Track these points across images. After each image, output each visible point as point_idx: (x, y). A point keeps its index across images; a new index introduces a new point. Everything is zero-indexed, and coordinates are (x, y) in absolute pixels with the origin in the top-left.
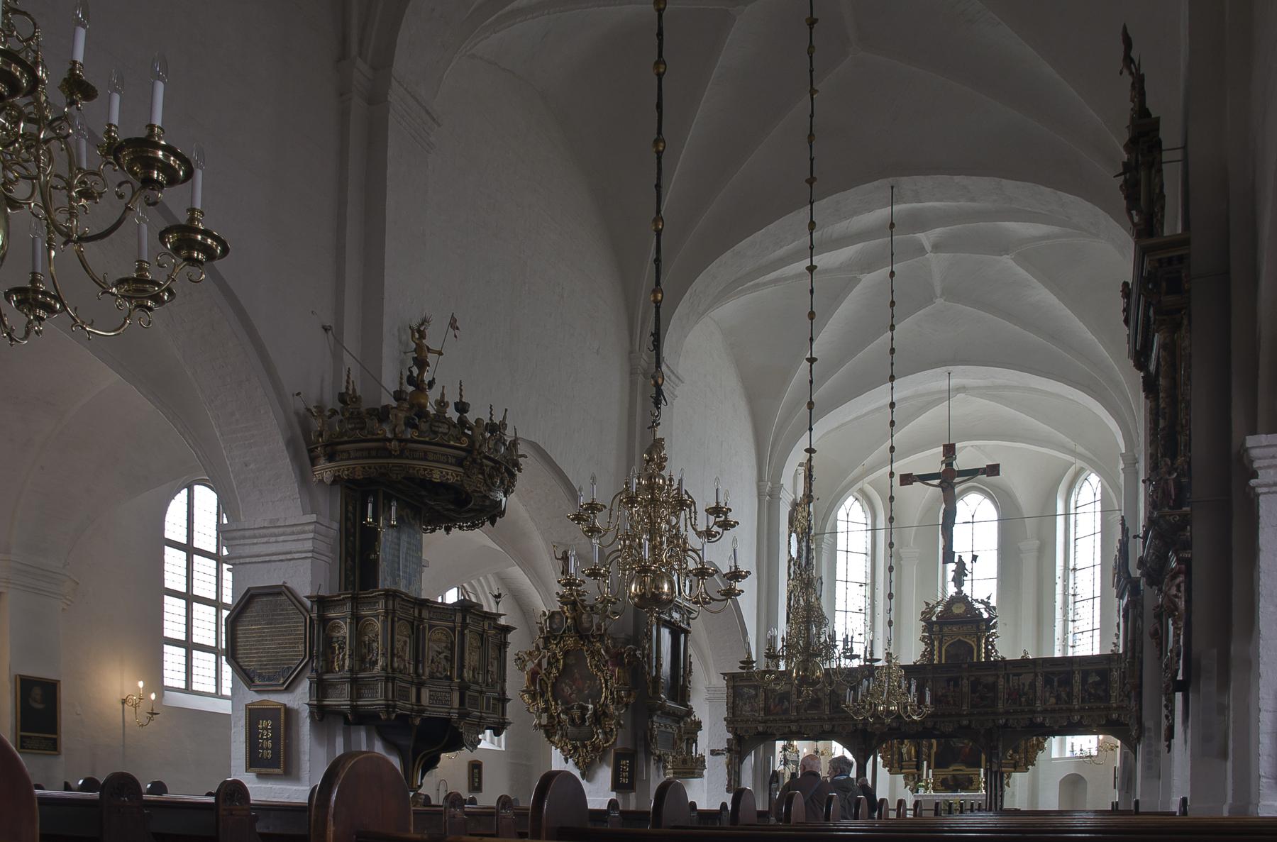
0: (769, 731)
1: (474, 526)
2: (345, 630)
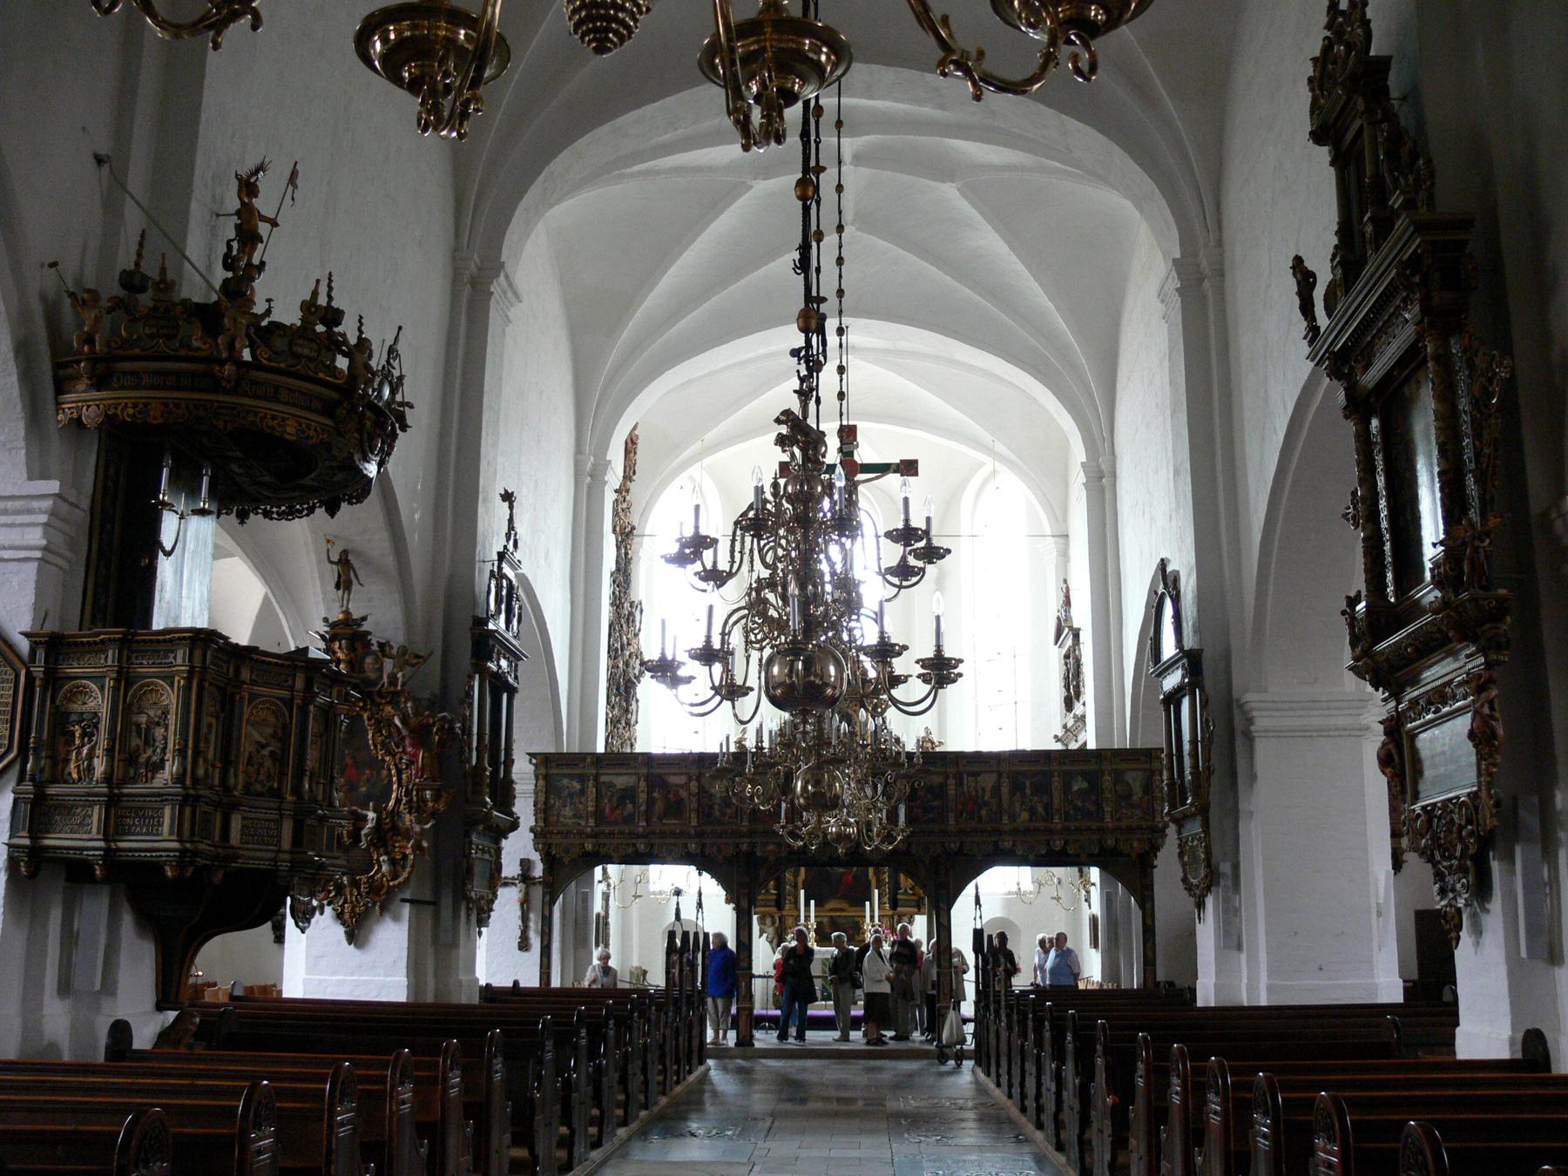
0: (603, 850)
1: (291, 514)
2: (98, 702)
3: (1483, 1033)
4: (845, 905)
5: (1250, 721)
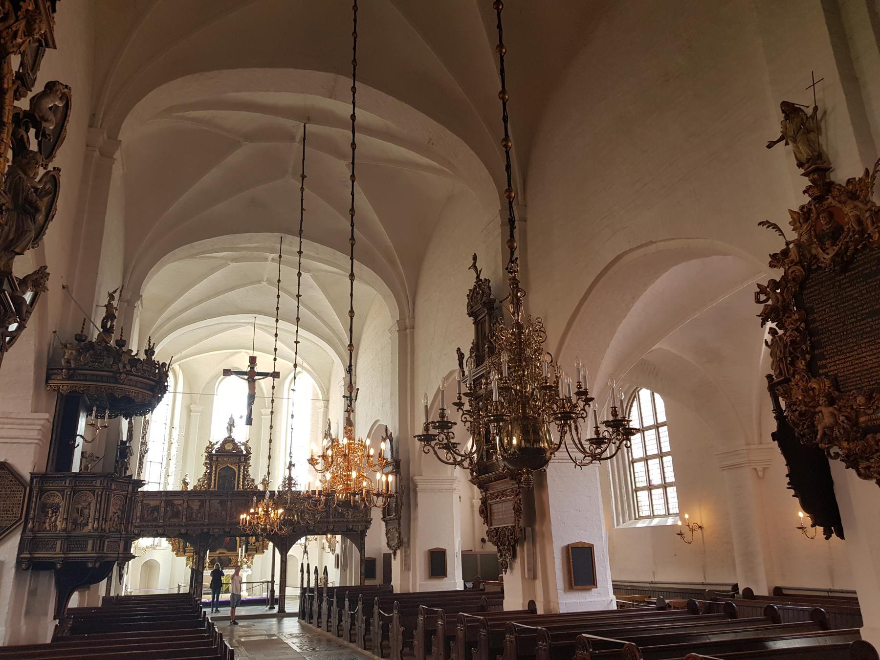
3: (513, 602)
4: (225, 551)
5: (416, 486)
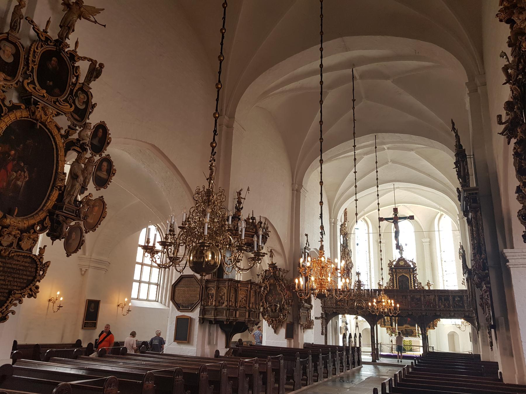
2: (213, 291)
4: (409, 326)
